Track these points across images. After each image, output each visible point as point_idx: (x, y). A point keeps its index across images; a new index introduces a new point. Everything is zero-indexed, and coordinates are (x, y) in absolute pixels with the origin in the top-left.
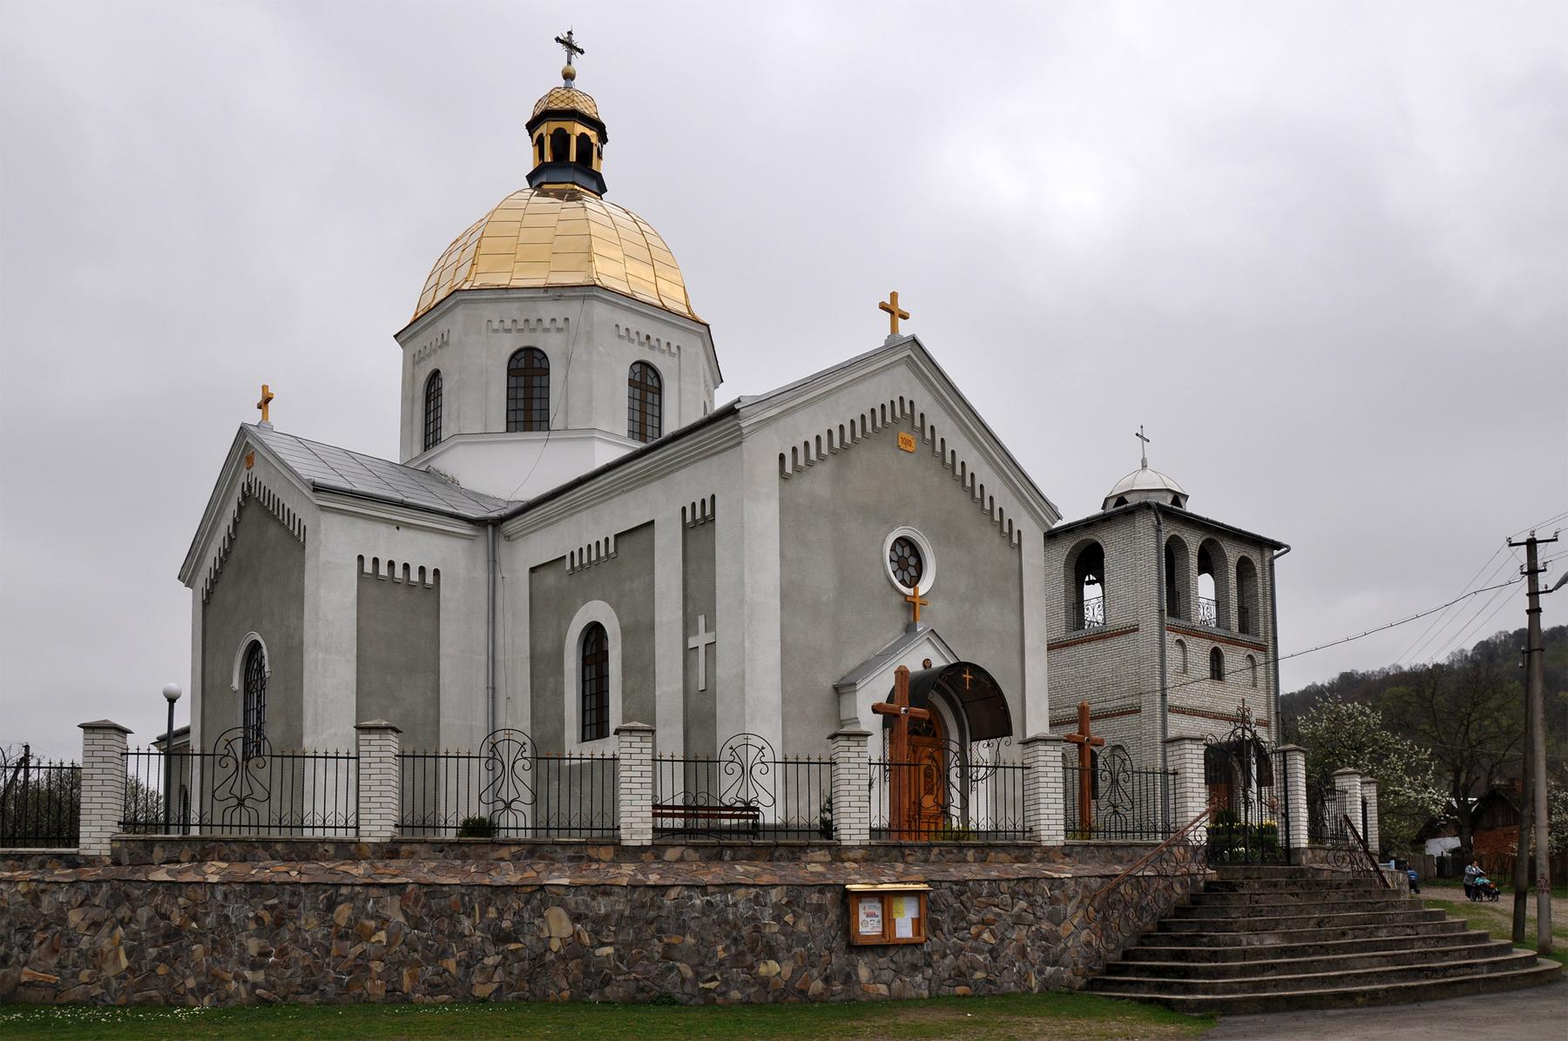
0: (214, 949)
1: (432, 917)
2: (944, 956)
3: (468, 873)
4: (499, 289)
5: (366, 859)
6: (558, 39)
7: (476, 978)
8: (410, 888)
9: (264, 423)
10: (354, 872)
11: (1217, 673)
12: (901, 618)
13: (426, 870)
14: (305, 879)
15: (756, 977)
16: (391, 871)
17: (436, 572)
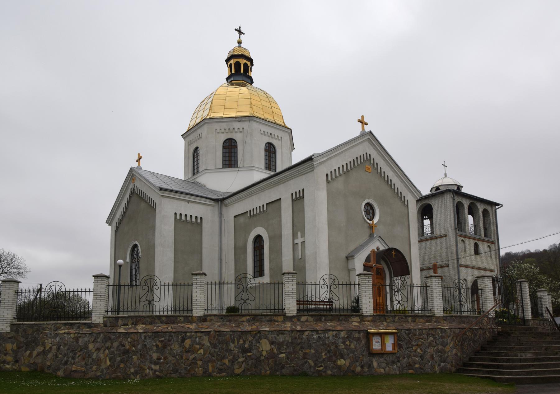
0: (141, 357)
1: (219, 344)
2: (404, 358)
3: (232, 327)
4: (219, 118)
5: (195, 322)
6: (236, 30)
7: (236, 366)
8: (212, 333)
9: (139, 167)
10: (191, 327)
11: (477, 252)
12: (368, 231)
13: (217, 326)
14: (174, 330)
15: (337, 365)
16: (204, 326)
17: (201, 218)
